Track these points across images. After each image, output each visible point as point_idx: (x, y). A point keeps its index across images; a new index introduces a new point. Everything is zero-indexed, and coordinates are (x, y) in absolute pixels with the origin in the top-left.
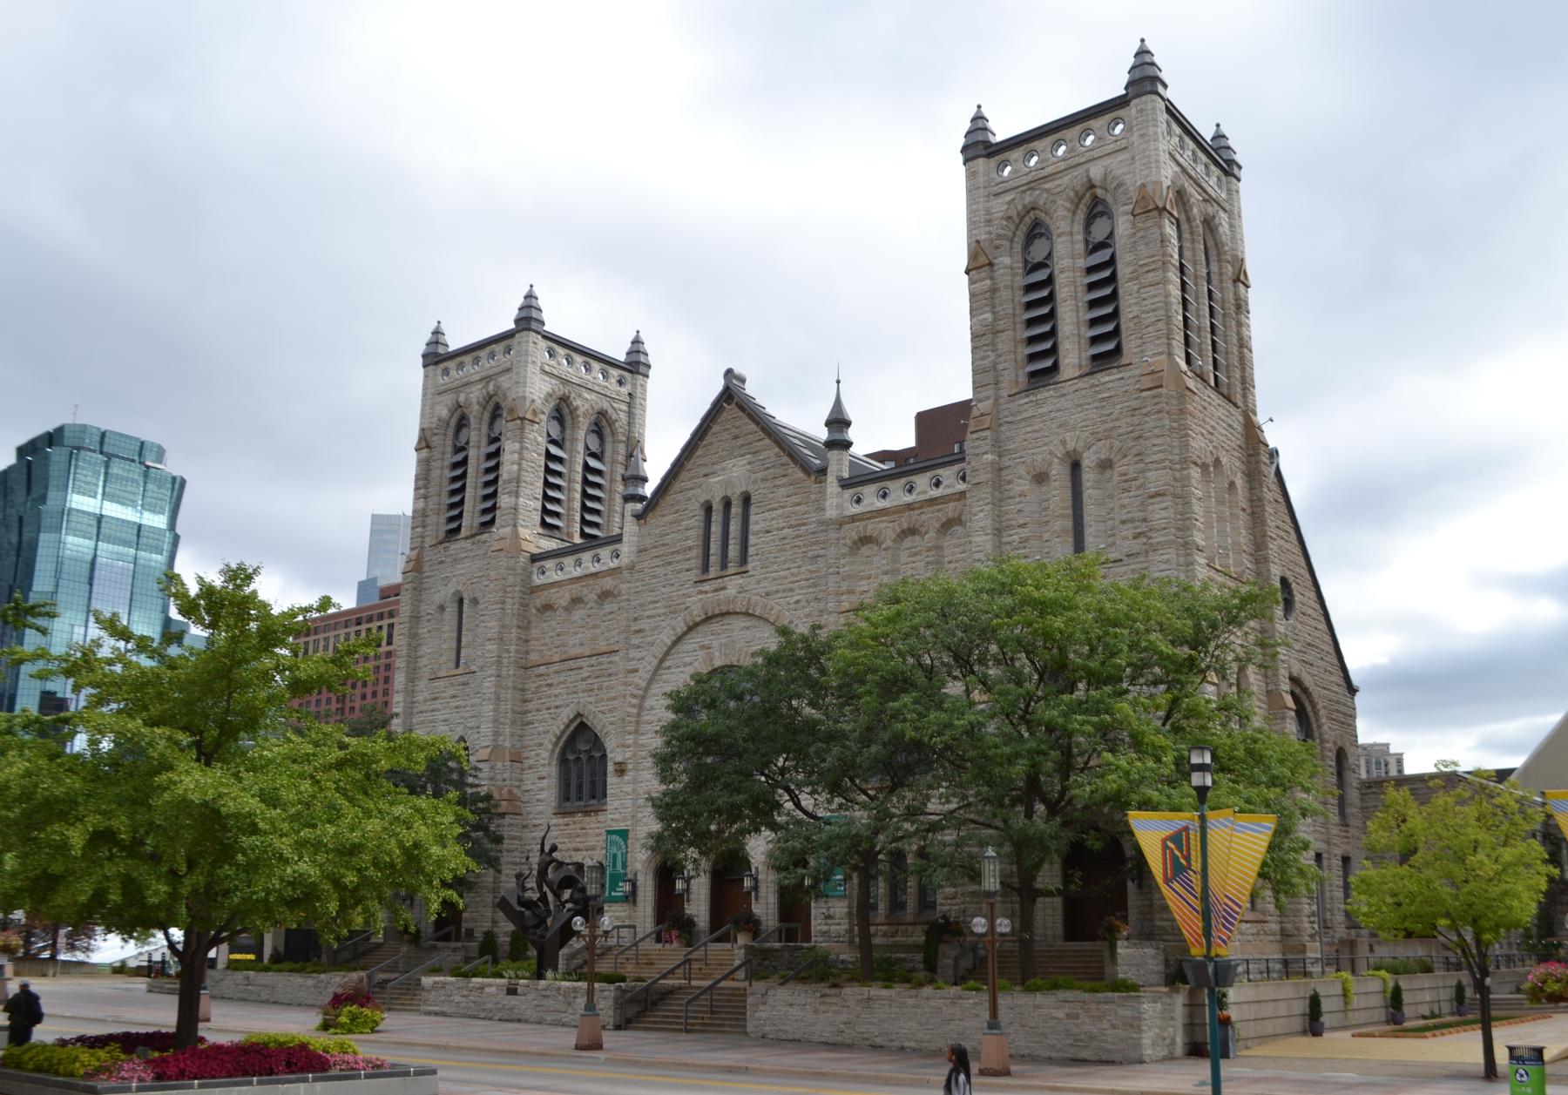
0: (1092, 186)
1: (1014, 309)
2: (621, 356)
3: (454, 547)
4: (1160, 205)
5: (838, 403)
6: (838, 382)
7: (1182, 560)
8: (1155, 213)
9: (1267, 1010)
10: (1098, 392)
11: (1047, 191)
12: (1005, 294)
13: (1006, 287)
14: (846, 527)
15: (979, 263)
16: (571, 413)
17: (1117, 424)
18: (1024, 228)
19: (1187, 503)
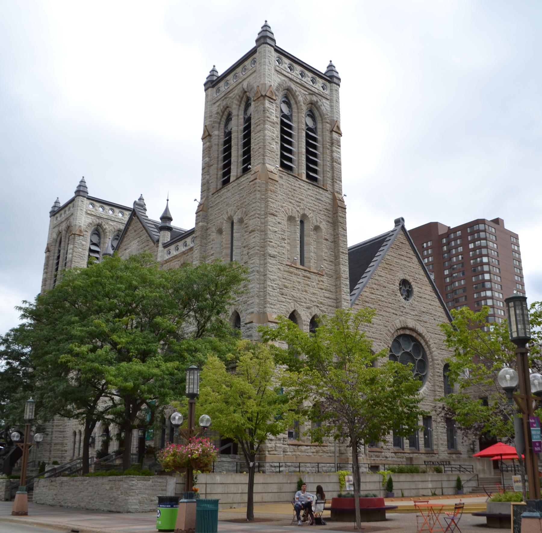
0: (245, 92)
1: (218, 154)
2: (323, 70)
3: (230, 186)
4: (264, 94)
5: (167, 210)
6: (168, 200)
7: (262, 262)
8: (262, 98)
9: (233, 489)
10: (239, 187)
11: (231, 97)
12: (215, 148)
13: (215, 145)
14: (164, 265)
15: (207, 136)
16: (103, 231)
17: (245, 200)
18: (225, 117)
19: (266, 234)
